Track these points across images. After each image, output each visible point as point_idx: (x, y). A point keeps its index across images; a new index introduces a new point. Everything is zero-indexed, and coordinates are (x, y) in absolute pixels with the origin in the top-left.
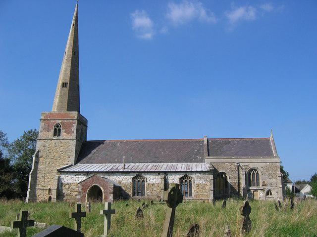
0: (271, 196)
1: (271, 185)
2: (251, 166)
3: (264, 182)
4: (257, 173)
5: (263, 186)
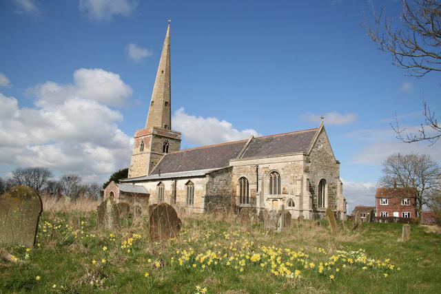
0: (293, 208)
1: (292, 194)
2: (272, 167)
3: (284, 189)
4: (279, 177)
5: (283, 193)
